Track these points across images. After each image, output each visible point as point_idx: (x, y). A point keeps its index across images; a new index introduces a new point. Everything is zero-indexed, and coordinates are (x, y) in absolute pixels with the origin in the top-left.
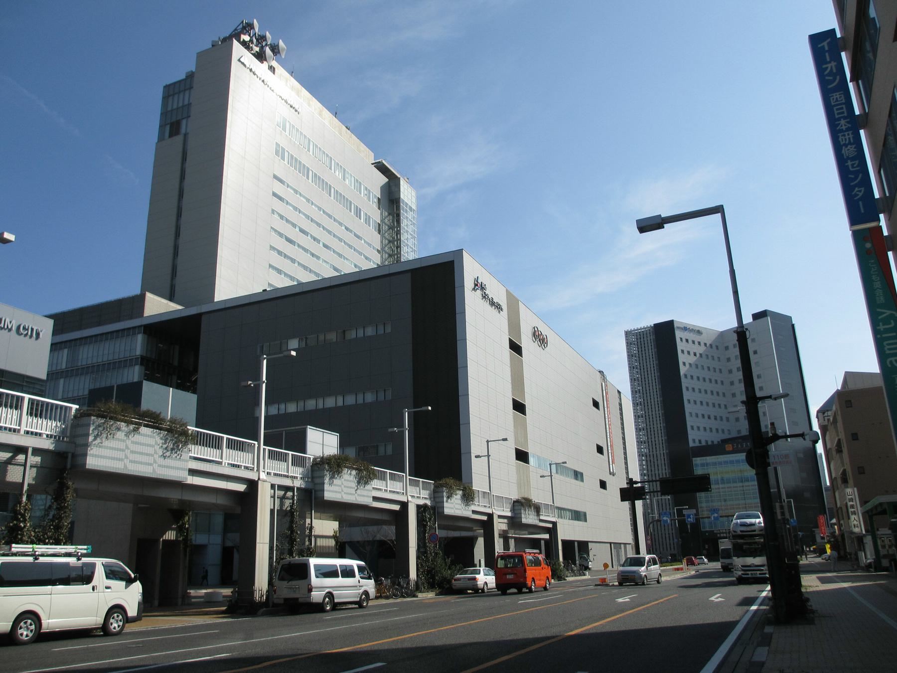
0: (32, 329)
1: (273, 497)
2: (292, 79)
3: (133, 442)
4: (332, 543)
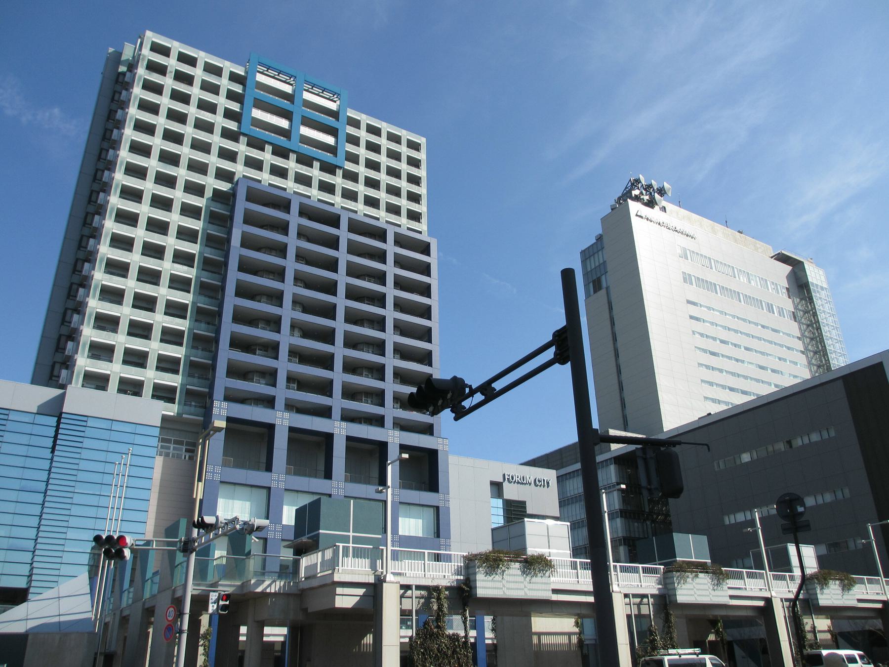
0: (544, 480)
1: (783, 607)
2: (682, 210)
3: (697, 584)
4: (828, 636)
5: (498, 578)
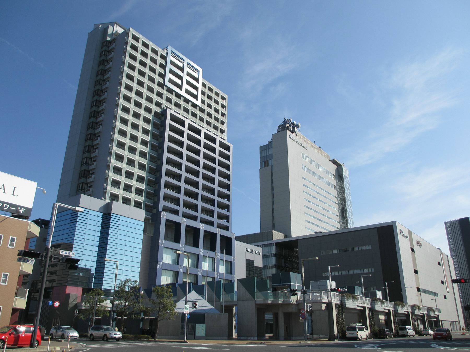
5: (349, 302)
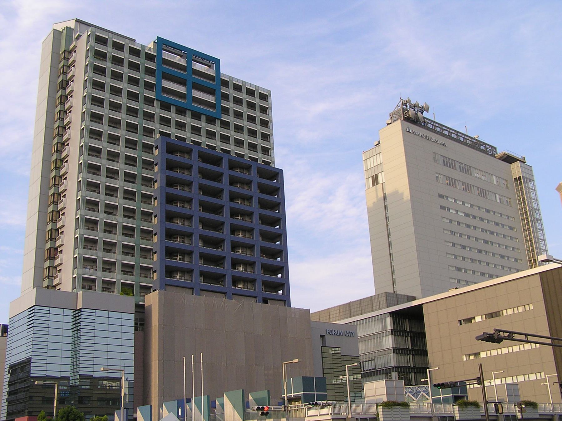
0: (350, 332)
